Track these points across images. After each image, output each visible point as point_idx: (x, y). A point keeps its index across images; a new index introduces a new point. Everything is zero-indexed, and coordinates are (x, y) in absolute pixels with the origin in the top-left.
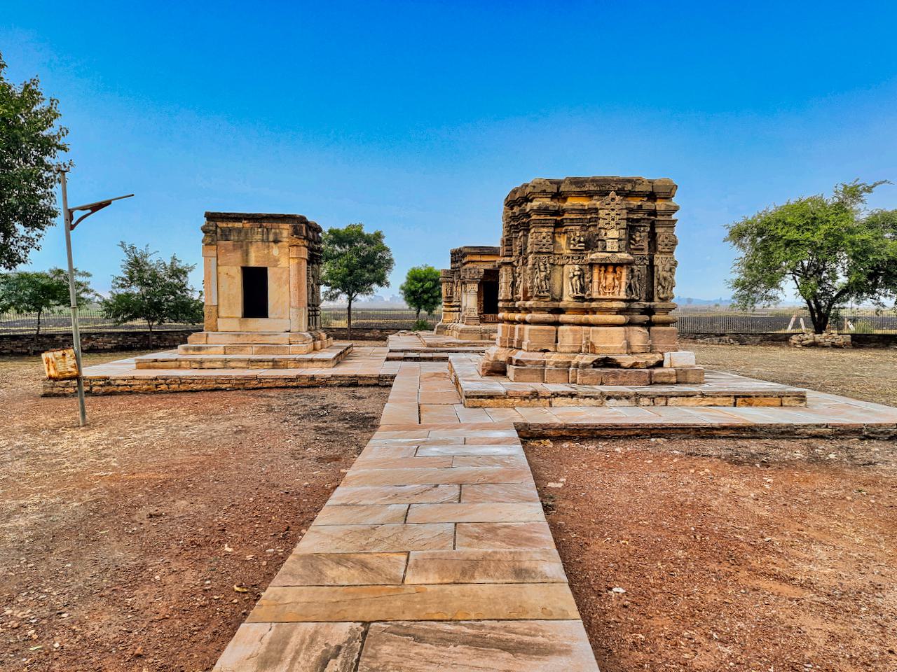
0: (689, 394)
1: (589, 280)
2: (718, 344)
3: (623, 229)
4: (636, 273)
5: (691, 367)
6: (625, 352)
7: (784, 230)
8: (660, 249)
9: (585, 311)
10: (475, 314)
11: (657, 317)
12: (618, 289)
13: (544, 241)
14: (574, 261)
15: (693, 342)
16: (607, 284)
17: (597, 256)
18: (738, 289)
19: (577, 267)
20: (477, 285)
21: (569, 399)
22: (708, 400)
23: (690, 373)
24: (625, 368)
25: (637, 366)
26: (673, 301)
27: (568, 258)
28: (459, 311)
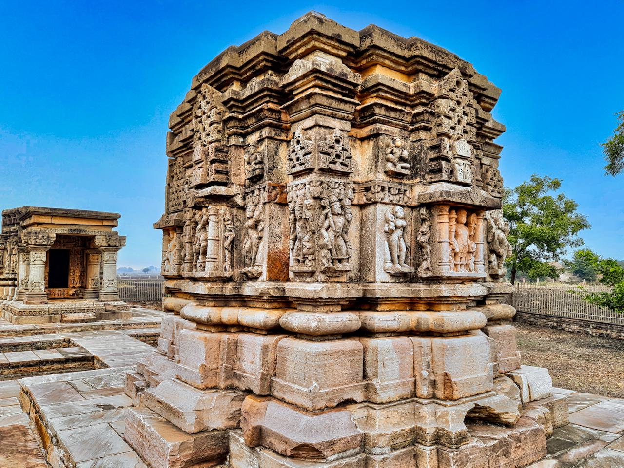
1: (426, 238)
10: (42, 288)
14: (392, 198)
20: (45, 253)
28: (15, 286)
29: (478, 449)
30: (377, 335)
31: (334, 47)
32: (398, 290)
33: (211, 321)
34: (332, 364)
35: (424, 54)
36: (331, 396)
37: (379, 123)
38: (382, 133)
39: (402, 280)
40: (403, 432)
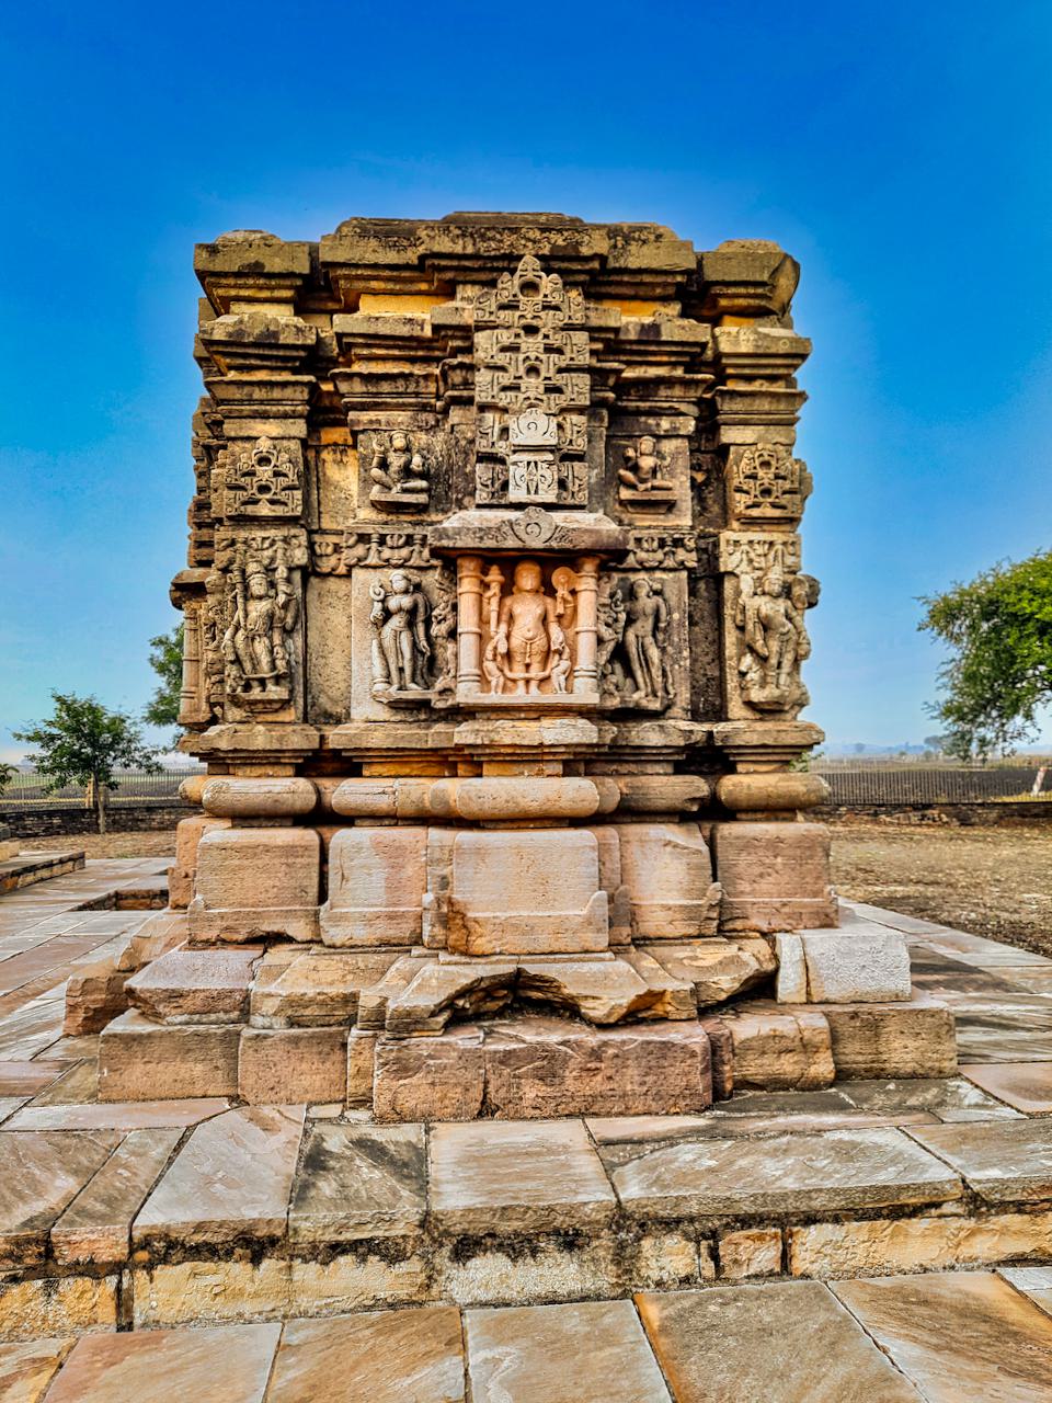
0: (905, 1199)
2: (920, 825)
3: (580, 410)
4: (646, 603)
5: (897, 999)
6: (604, 940)
7: (1035, 604)
8: (740, 508)
9: (449, 761)
11: (743, 783)
12: (565, 664)
13: (264, 473)
14: (387, 553)
15: (872, 821)
16: (516, 641)
17: (464, 523)
18: (950, 720)
19: (397, 578)
21: (237, 1271)
22: (1003, 1231)
23: (892, 1027)
24: (603, 1026)
25: (659, 1010)
26: (804, 716)
27: (363, 538)
29: (454, 1050)
30: (358, 822)
31: (261, 288)
32: (411, 734)
33: (187, 797)
34: (241, 868)
35: (436, 249)
36: (230, 923)
37: (355, 409)
38: (361, 428)
39: (423, 717)
40: (321, 997)
